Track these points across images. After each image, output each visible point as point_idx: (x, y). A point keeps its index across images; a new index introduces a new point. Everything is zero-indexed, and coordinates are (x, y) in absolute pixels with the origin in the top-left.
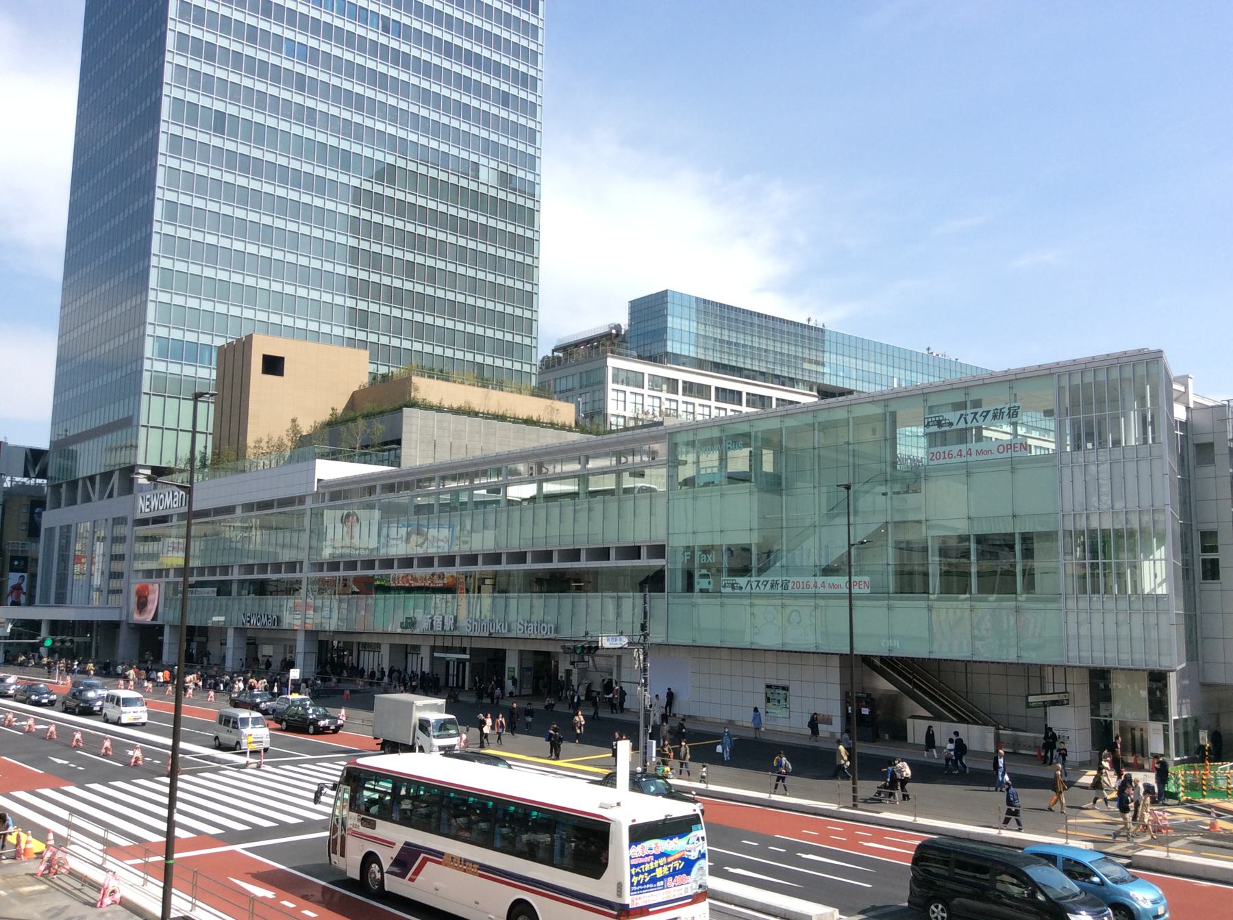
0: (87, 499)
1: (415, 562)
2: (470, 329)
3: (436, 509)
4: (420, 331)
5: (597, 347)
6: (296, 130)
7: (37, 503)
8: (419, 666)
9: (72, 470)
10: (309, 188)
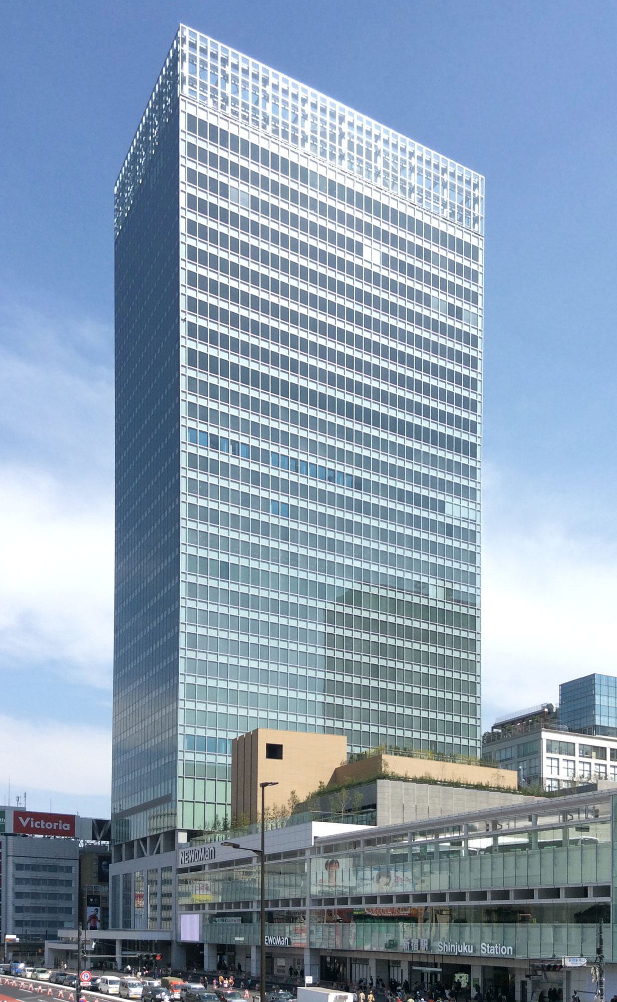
0: (141, 855)
1: (378, 900)
2: (424, 714)
4: (385, 719)
5: (532, 723)
6: (283, 571)
7: (104, 859)
8: (400, 976)
9: (127, 835)
10: (295, 615)
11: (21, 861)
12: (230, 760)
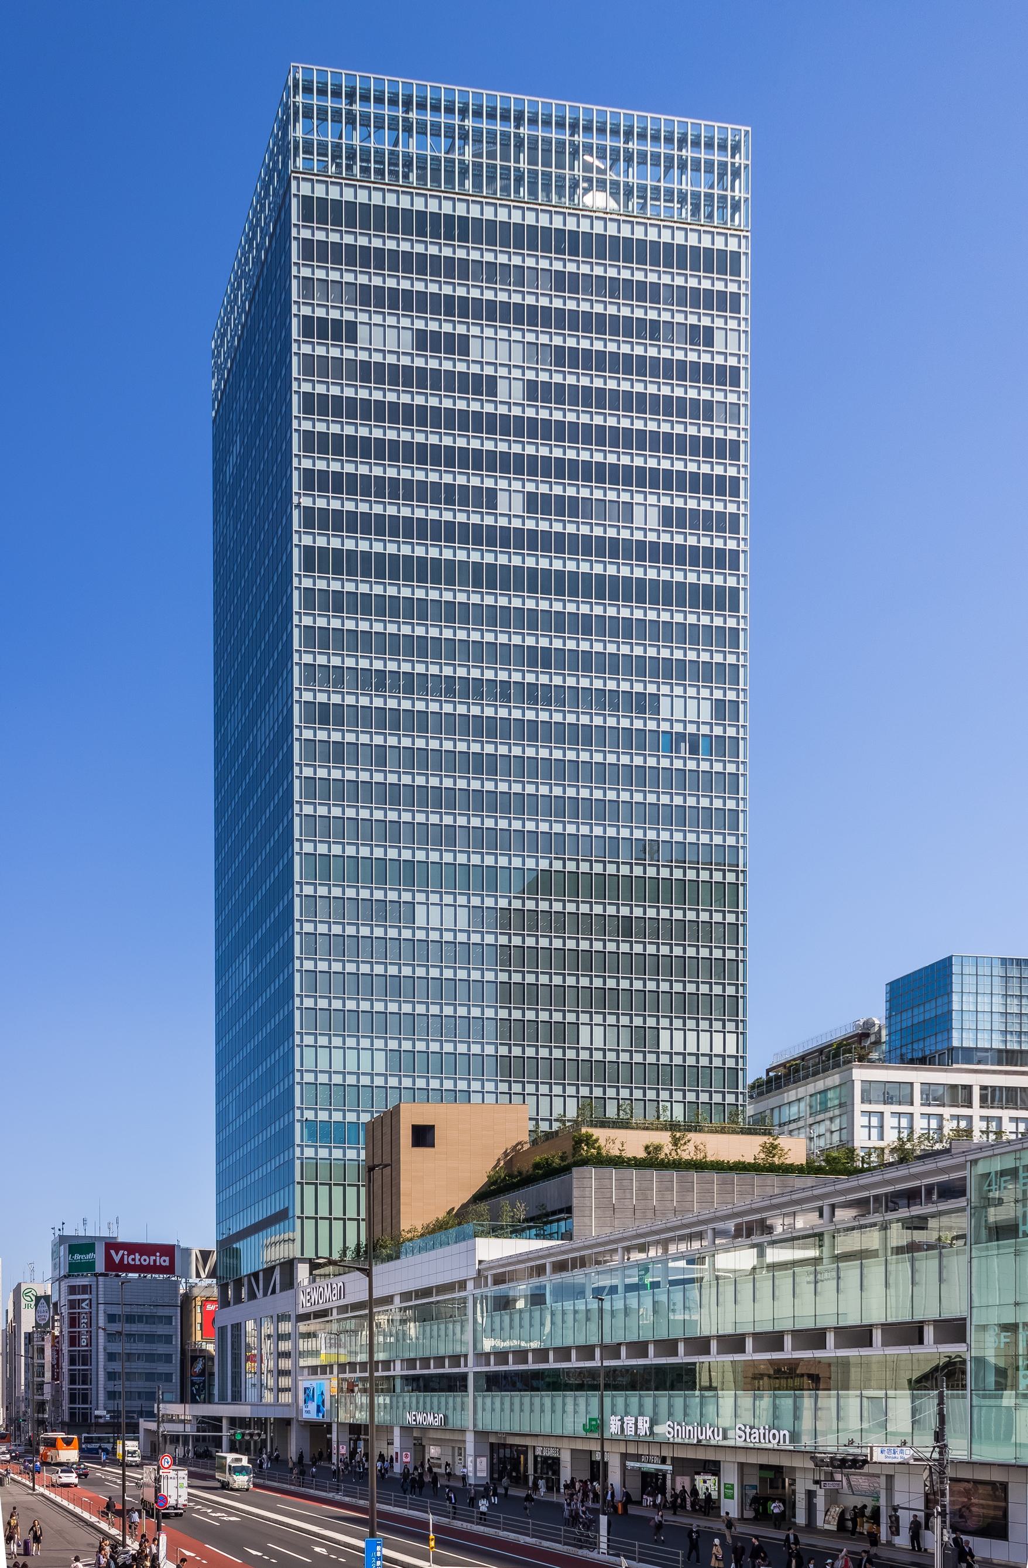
0: (252, 1296)
3: (621, 1289)
9: (237, 1268)
11: (116, 1310)
12: (363, 1155)
